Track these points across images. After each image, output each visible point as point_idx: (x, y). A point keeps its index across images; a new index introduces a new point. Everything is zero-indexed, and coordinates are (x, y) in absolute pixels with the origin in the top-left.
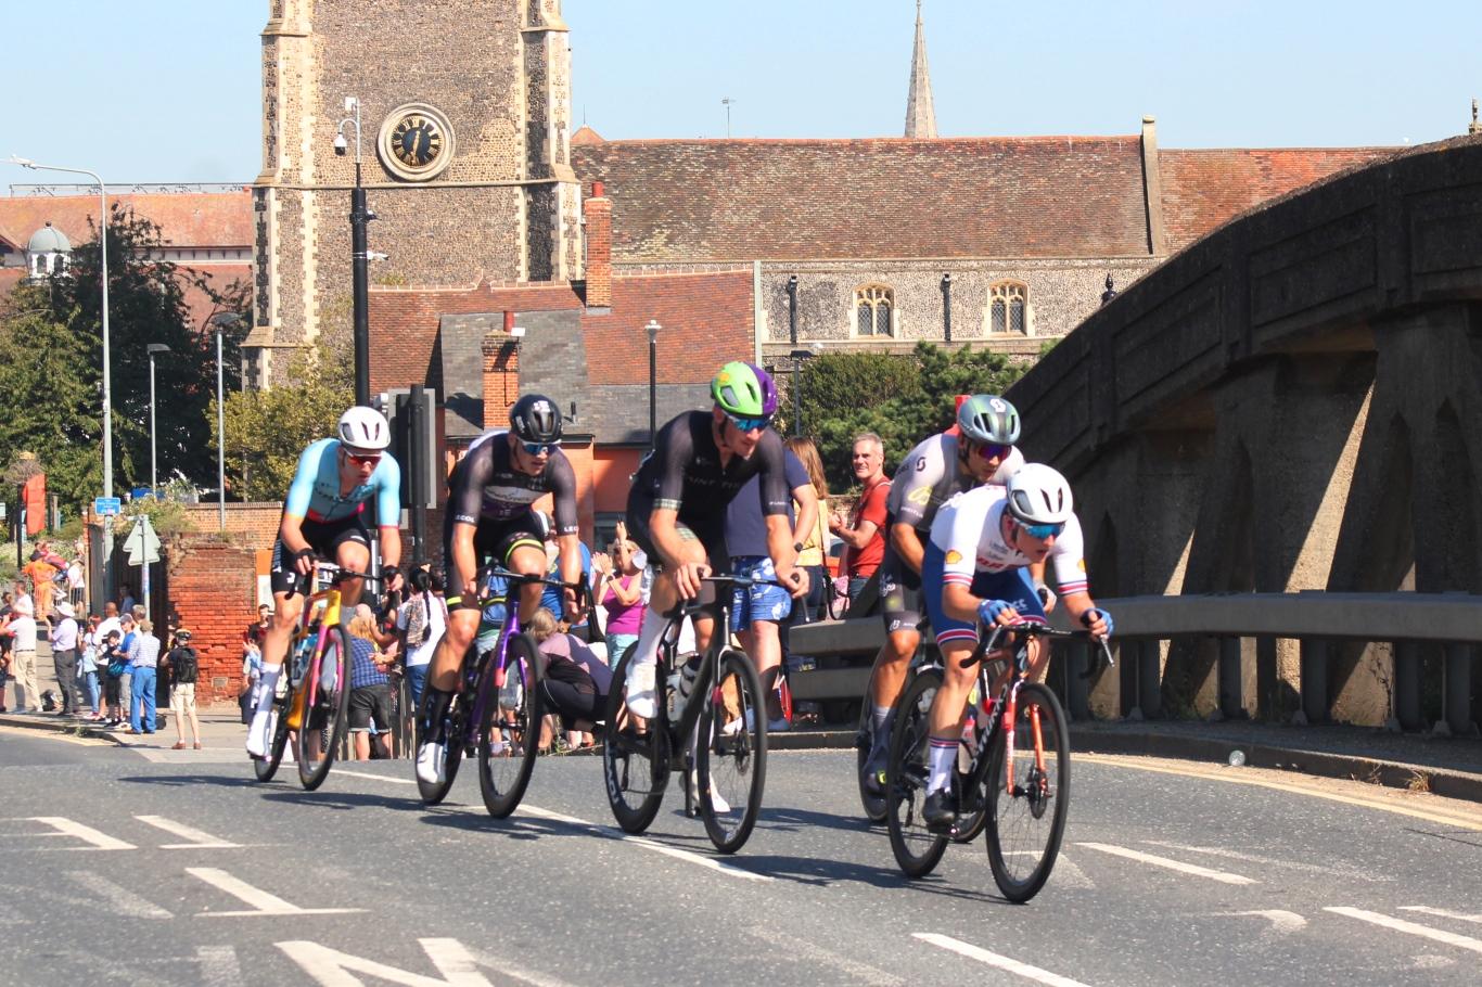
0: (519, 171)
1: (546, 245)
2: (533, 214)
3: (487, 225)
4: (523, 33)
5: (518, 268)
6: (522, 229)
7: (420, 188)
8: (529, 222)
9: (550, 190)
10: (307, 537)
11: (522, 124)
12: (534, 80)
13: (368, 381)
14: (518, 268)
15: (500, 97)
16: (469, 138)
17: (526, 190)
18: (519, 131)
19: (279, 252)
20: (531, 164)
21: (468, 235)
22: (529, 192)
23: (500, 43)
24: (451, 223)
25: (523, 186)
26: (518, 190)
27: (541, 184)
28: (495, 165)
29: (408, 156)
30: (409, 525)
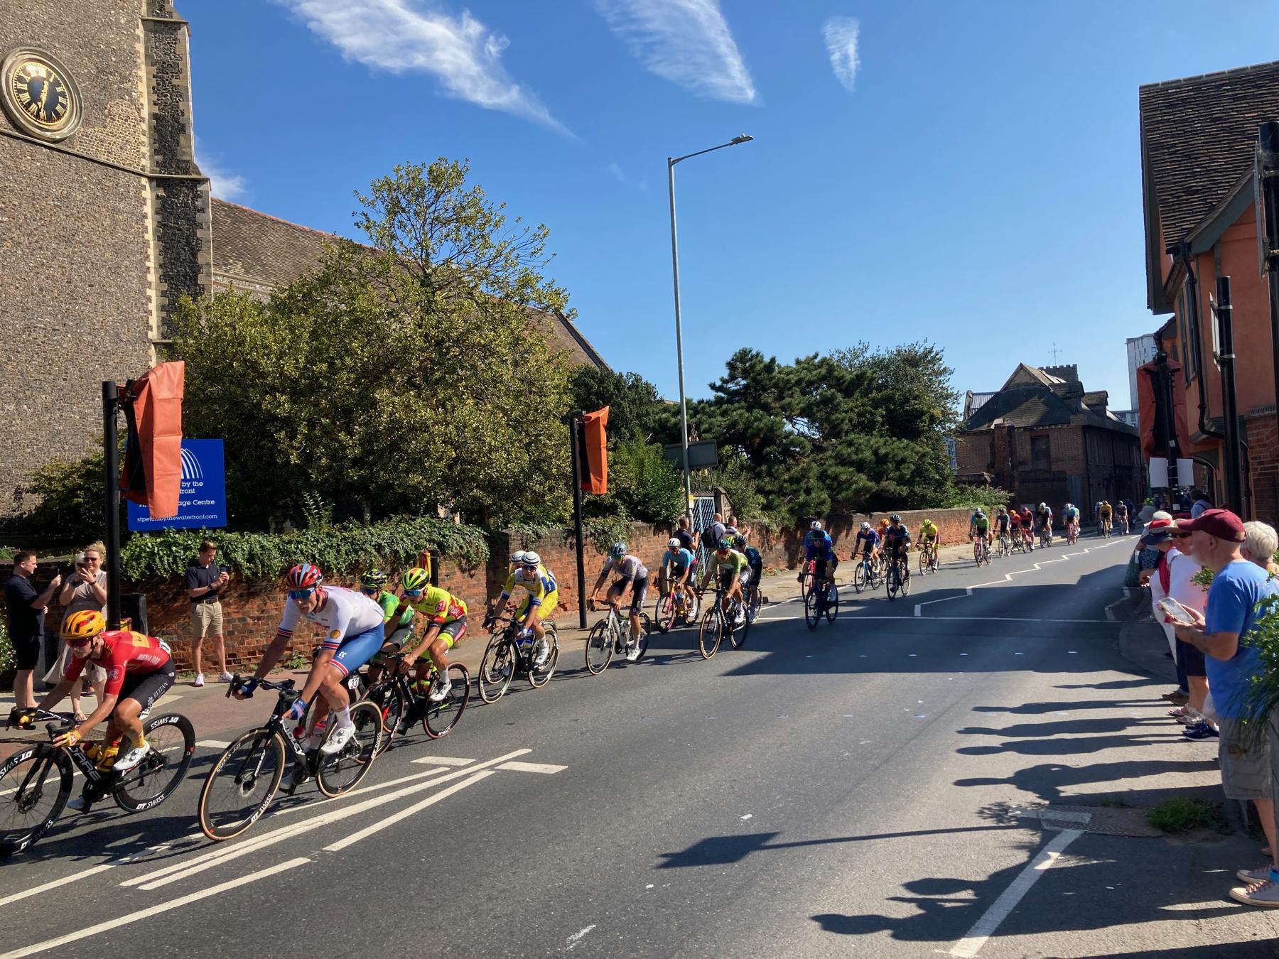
0: (143, 162)
1: (188, 243)
2: (163, 208)
3: (115, 210)
4: (143, 20)
5: (148, 264)
6: (150, 223)
7: (46, 147)
8: (159, 218)
9: (196, 186)
10: (1045, 799)
11: (145, 113)
12: (161, 70)
13: (574, 463)
14: (148, 264)
15: (125, 79)
16: (94, 111)
17: (154, 183)
18: (143, 120)
19: (145, 216)
20: (159, 158)
21: (97, 215)
22: (158, 186)
23: (122, 21)
24: (79, 198)
25: (150, 179)
26: (144, 181)
27: (181, 179)
28: (122, 148)
29: (34, 106)
30: (1223, 779)
